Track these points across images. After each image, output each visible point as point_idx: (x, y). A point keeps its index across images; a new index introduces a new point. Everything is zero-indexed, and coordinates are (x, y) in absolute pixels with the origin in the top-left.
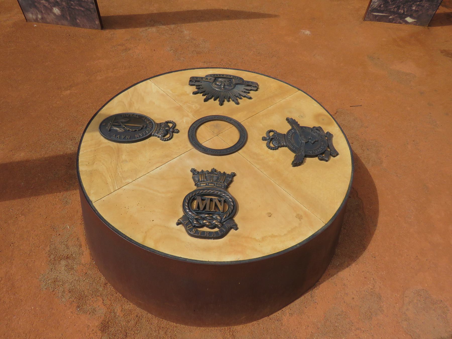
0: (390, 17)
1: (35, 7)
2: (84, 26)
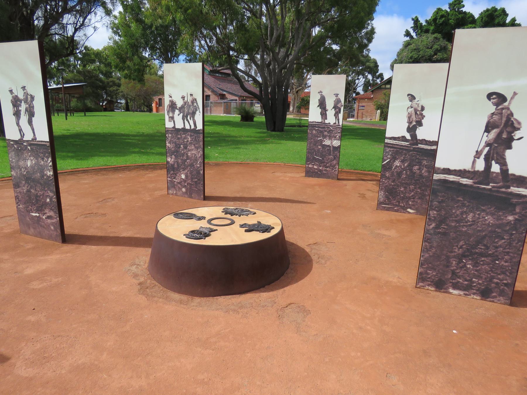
0: (395, 208)
1: (175, 187)
2: (195, 199)
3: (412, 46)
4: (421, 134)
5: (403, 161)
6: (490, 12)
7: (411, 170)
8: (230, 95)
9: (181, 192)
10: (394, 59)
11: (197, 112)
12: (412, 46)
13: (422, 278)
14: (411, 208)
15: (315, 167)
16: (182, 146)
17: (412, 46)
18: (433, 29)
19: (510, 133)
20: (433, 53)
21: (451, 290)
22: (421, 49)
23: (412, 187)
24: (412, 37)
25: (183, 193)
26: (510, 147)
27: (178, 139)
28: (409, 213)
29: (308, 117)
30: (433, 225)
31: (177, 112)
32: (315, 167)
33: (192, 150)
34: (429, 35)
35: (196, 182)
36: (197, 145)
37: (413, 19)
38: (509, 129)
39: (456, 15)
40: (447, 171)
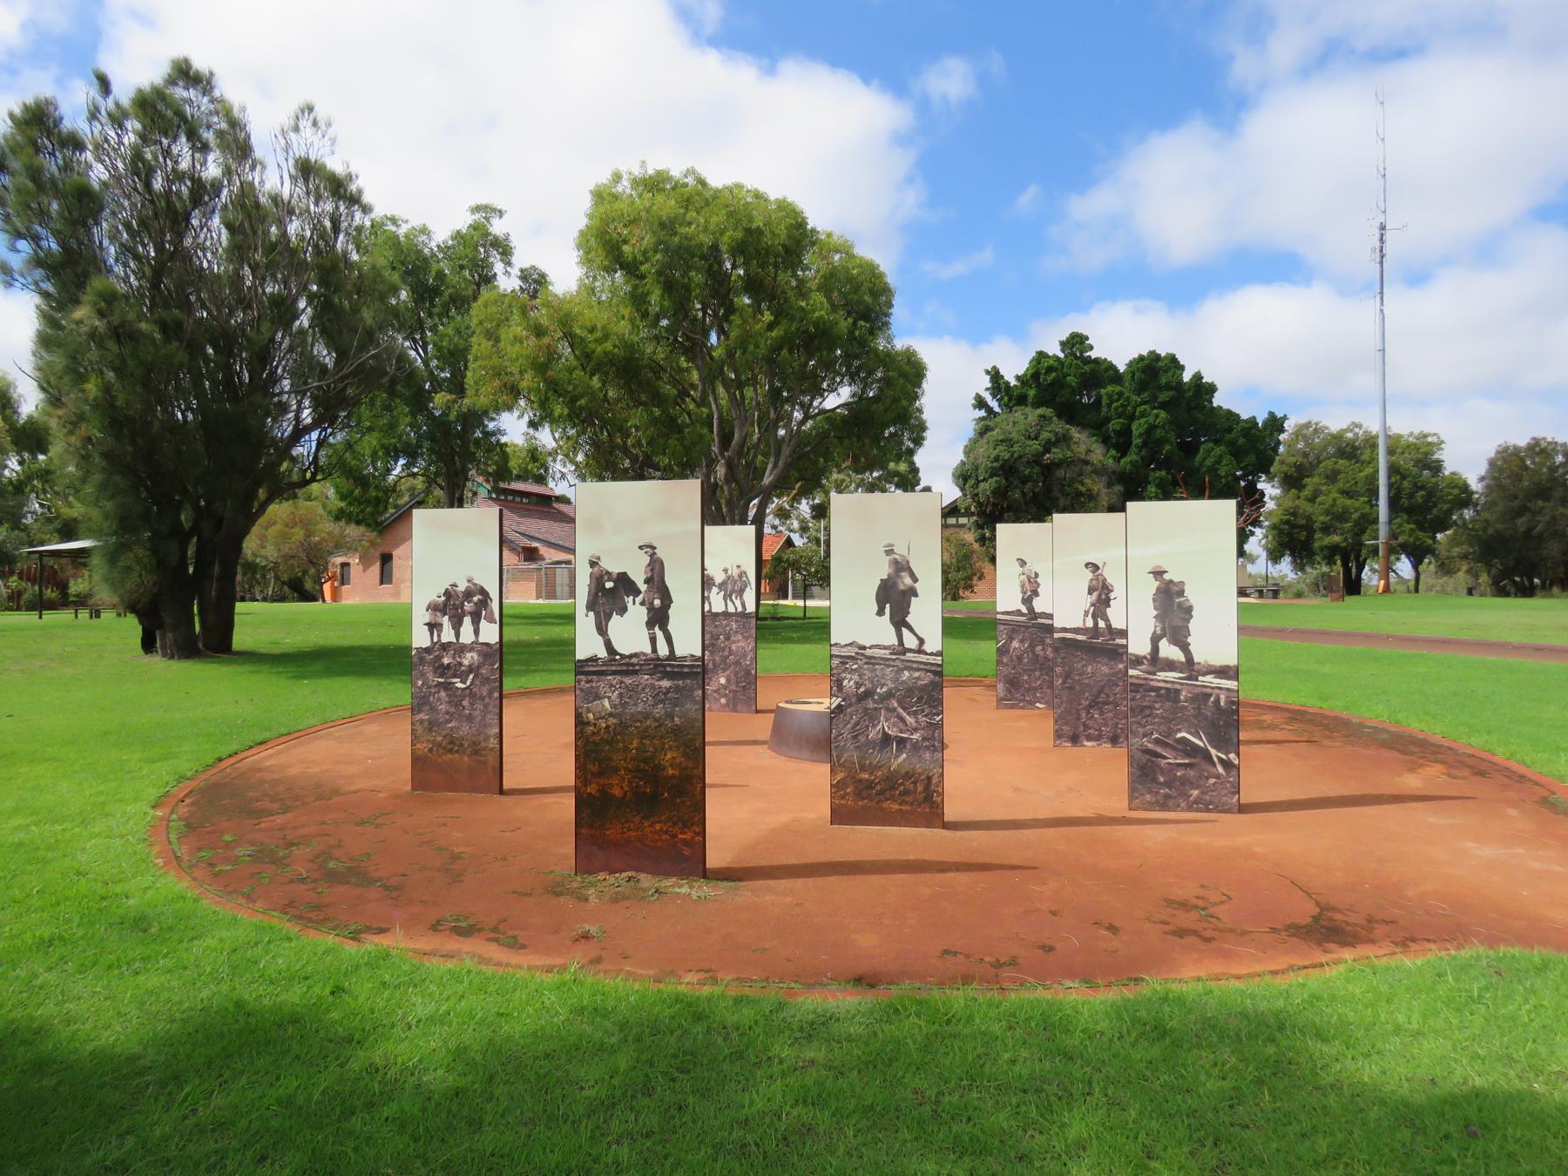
3: (995, 434)
4: (1039, 605)
5: (1022, 641)
6: (1145, 362)
7: (1033, 652)
8: (552, 550)
9: (718, 705)
10: (959, 462)
11: (748, 589)
12: (995, 434)
13: (1058, 735)
14: (1040, 703)
16: (721, 637)
17: (994, 433)
18: (1035, 395)
19: (1107, 595)
20: (1041, 449)
21: (1086, 743)
22: (1016, 440)
23: (1037, 673)
24: (990, 411)
25: (723, 706)
26: (1109, 606)
27: (716, 626)
28: (1039, 708)
30: (1060, 681)
31: (715, 590)
33: (739, 641)
34: (1028, 410)
35: (744, 687)
36: (746, 635)
37: (988, 372)
38: (1106, 591)
39: (1078, 367)
40: (1064, 630)
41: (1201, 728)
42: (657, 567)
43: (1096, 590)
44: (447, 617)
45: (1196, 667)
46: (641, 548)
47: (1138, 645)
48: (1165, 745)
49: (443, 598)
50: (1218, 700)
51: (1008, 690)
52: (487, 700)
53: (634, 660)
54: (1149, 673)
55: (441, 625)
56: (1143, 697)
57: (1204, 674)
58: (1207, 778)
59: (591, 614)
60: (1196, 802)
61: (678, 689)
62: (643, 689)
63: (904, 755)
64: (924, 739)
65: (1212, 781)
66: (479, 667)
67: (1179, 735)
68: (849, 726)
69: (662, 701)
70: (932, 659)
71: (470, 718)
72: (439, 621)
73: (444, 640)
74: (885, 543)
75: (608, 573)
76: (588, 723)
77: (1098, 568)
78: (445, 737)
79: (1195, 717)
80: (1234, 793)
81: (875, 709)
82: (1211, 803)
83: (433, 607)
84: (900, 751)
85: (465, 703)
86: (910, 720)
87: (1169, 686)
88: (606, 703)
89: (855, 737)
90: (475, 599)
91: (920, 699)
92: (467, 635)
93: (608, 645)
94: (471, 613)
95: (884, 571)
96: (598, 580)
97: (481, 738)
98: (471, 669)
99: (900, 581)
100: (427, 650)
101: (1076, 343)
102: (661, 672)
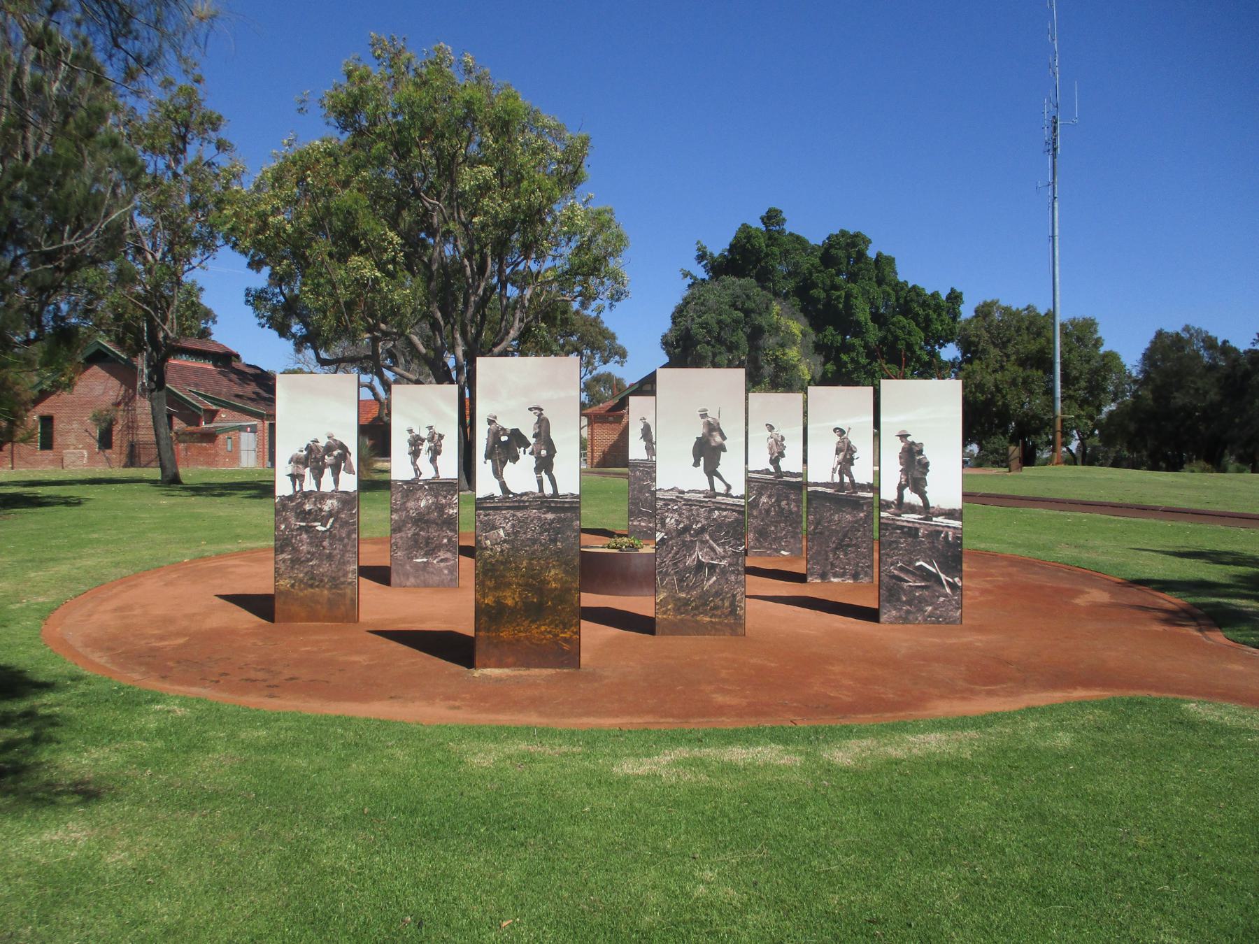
5: (770, 497)
7: (779, 506)
15: (643, 524)
19: (851, 455)
29: (390, 461)
32: (643, 524)
40: (816, 484)
41: (934, 558)
42: (544, 424)
43: (842, 451)
44: (308, 469)
45: (931, 510)
46: (530, 409)
47: (889, 492)
48: (907, 572)
49: (305, 453)
50: (947, 536)
51: (757, 539)
52: (346, 541)
53: (525, 498)
54: (896, 515)
55: (303, 476)
56: (891, 534)
57: (937, 516)
58: (938, 597)
59: (489, 461)
60: (929, 616)
61: (559, 520)
62: (532, 521)
63: (714, 578)
64: (730, 565)
65: (942, 599)
66: (338, 512)
67: (918, 564)
68: (670, 555)
69: (546, 530)
70: (736, 501)
71: (330, 557)
72: (301, 472)
73: (306, 488)
74: (700, 408)
75: (503, 429)
76: (486, 548)
77: (844, 432)
78: (306, 574)
79: (930, 549)
80: (957, 609)
81: (691, 541)
82: (941, 617)
83: (296, 461)
84: (711, 575)
85: (326, 543)
86: (719, 550)
87: (910, 525)
88: (501, 532)
89: (675, 564)
90: (335, 453)
91: (727, 533)
92: (327, 484)
93: (503, 486)
94: (331, 465)
95: (699, 431)
96: (495, 435)
97: (341, 574)
98: (331, 514)
99: (711, 439)
100: (290, 498)
101: (772, 217)
102: (547, 507)
